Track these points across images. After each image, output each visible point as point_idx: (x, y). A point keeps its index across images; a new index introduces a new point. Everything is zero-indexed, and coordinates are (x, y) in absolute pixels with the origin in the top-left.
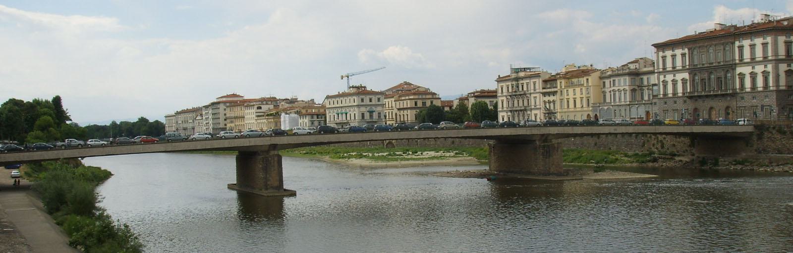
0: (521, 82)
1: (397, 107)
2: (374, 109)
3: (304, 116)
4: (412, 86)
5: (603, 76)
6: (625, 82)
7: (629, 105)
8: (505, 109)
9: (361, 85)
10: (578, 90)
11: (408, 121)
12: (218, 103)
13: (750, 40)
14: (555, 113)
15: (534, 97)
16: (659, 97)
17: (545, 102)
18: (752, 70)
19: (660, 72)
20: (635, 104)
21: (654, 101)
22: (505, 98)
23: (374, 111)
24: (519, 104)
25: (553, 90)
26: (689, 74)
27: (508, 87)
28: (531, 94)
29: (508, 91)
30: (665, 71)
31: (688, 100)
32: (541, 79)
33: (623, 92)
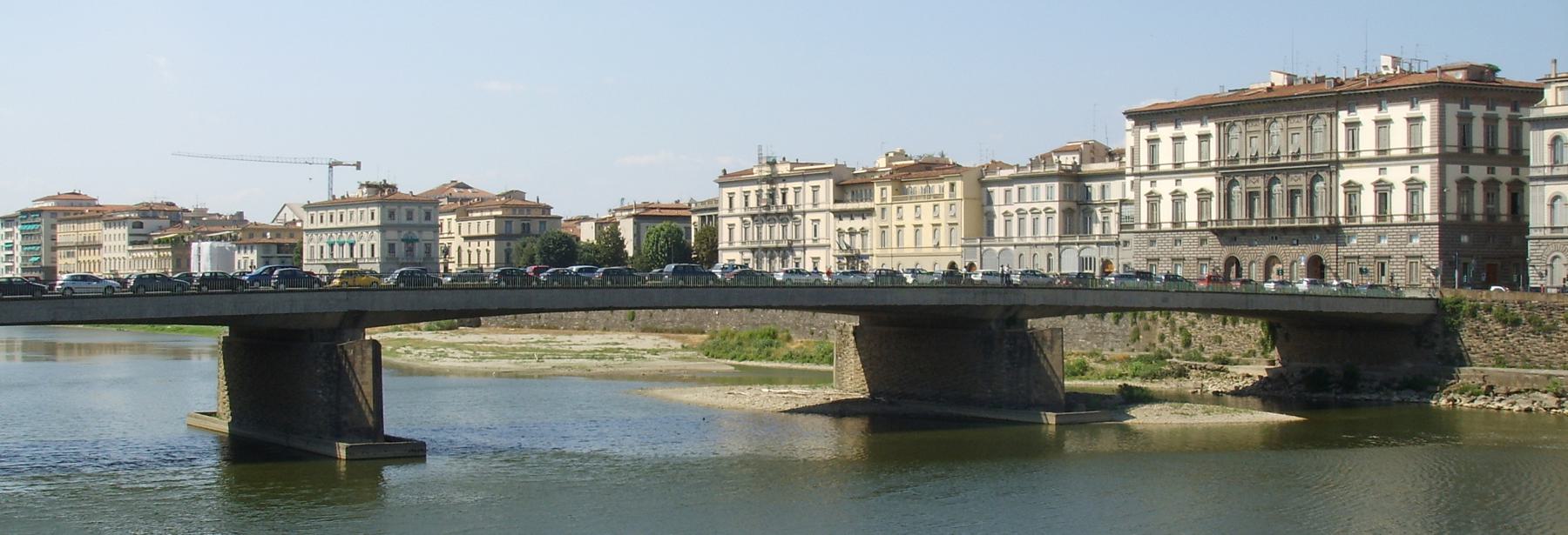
0: (781, 185)
1: (463, 234)
2: (416, 234)
3: (249, 247)
4: (470, 190)
5: (982, 183)
6: (1049, 198)
7: (1059, 245)
8: (738, 245)
9: (385, 181)
10: (927, 208)
11: (488, 264)
12: (39, 212)
13: (1199, 125)
14: (867, 257)
15: (813, 221)
16: (1136, 228)
17: (840, 232)
18: (1175, 188)
19: (1141, 175)
20: (1073, 244)
21: (1124, 237)
22: (737, 221)
23: (417, 240)
24: (774, 234)
25: (862, 205)
26: (1219, 180)
27: (746, 197)
28: (804, 213)
29: (746, 204)
30: (1154, 171)
31: (1212, 238)
32: (831, 181)
33: (1043, 217)
